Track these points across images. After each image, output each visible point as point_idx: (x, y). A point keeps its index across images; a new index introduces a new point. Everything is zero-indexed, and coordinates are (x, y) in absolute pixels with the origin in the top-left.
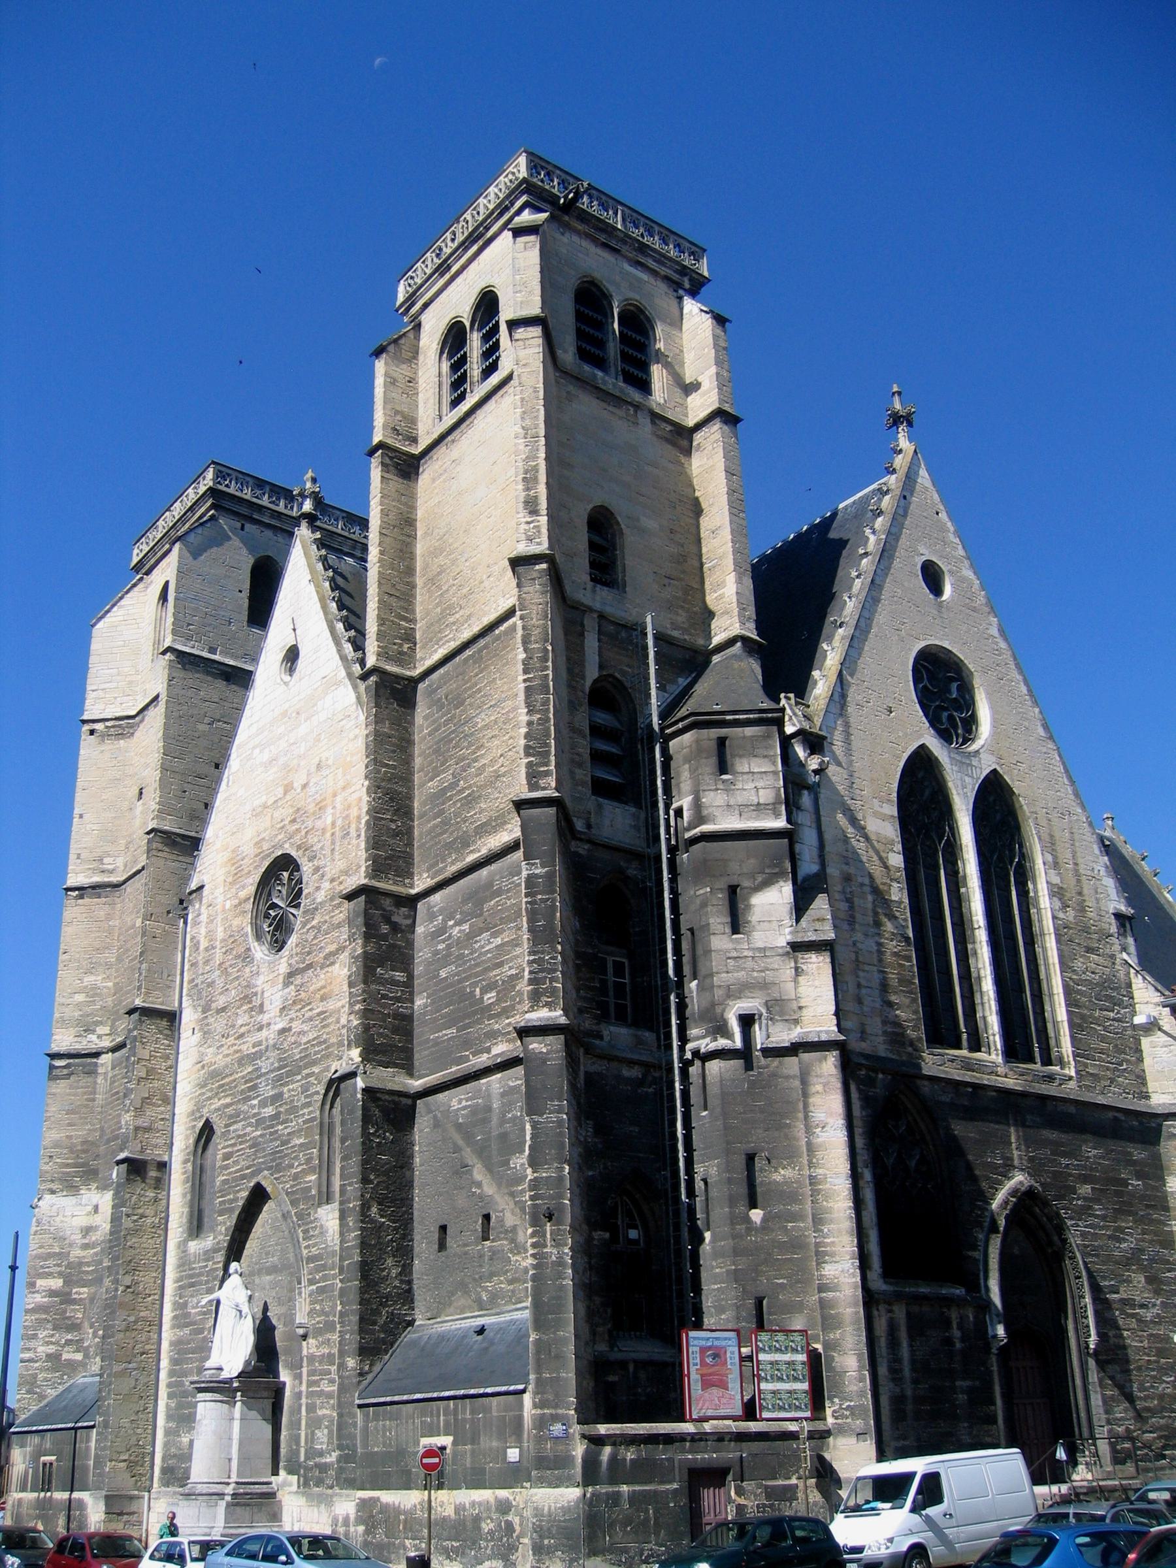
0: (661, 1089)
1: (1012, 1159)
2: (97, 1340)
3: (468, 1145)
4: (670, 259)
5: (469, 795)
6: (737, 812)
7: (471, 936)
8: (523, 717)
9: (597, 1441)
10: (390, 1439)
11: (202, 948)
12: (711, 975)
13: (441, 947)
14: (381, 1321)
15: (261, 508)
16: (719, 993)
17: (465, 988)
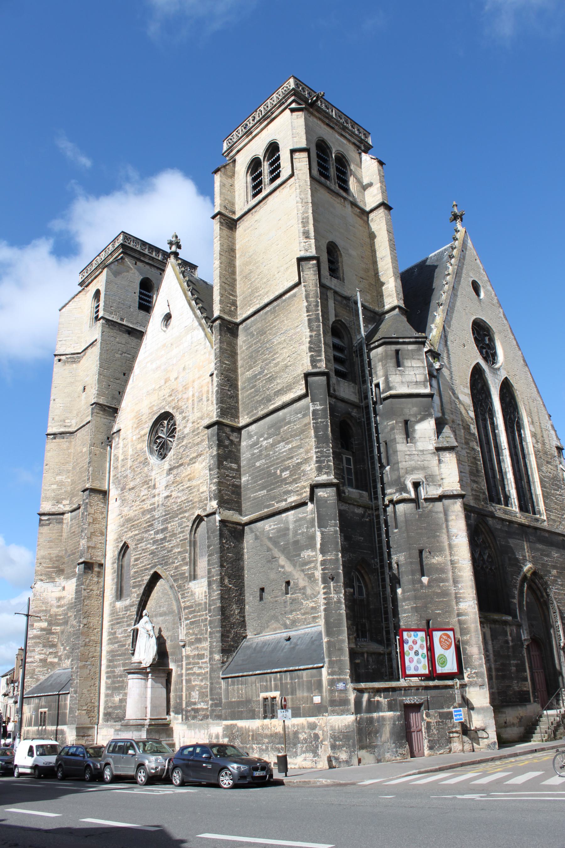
0: (373, 519)
1: (525, 556)
2: (66, 652)
3: (276, 547)
4: (356, 135)
5: (270, 377)
6: (406, 385)
7: (273, 445)
8: (307, 332)
9: (361, 691)
10: (242, 694)
11: (120, 459)
12: (398, 463)
13: (256, 451)
14: (231, 636)
15: (144, 255)
16: (402, 472)
17: (271, 470)
